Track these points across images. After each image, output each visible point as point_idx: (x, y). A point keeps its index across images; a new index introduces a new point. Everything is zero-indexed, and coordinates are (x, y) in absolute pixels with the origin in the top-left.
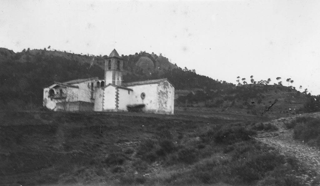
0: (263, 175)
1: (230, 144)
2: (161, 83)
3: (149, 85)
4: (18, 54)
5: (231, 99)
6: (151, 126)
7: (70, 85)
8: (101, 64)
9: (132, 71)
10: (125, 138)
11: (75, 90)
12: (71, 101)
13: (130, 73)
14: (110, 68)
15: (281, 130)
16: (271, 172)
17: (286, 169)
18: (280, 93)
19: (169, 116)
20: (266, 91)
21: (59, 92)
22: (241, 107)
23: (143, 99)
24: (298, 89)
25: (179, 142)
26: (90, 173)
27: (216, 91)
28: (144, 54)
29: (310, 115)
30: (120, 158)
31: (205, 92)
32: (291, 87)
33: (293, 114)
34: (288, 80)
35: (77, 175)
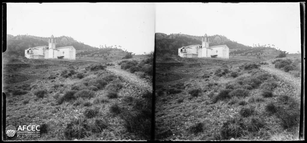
0: (263, 82)
1: (251, 70)
2: (224, 47)
3: (219, 47)
4: (15, 37)
5: (251, 53)
6: (220, 63)
7: (188, 47)
8: (201, 39)
9: (213, 42)
10: (210, 68)
11: (37, 50)
12: (189, 53)
13: (212, 43)
14: (51, 42)
15: (116, 66)
16: (266, 80)
17: (272, 79)
18: (269, 50)
19: (227, 59)
20: (264, 49)
21: (31, 51)
22: (255, 56)
23: (63, 54)
24: (123, 50)
25: (231, 69)
26: (196, 81)
27: (245, 50)
28: (217, 35)
29: (127, 60)
30: (54, 76)
31: (241, 50)
32: (120, 49)
33: (275, 58)
34: (119, 46)
35: (38, 83)
